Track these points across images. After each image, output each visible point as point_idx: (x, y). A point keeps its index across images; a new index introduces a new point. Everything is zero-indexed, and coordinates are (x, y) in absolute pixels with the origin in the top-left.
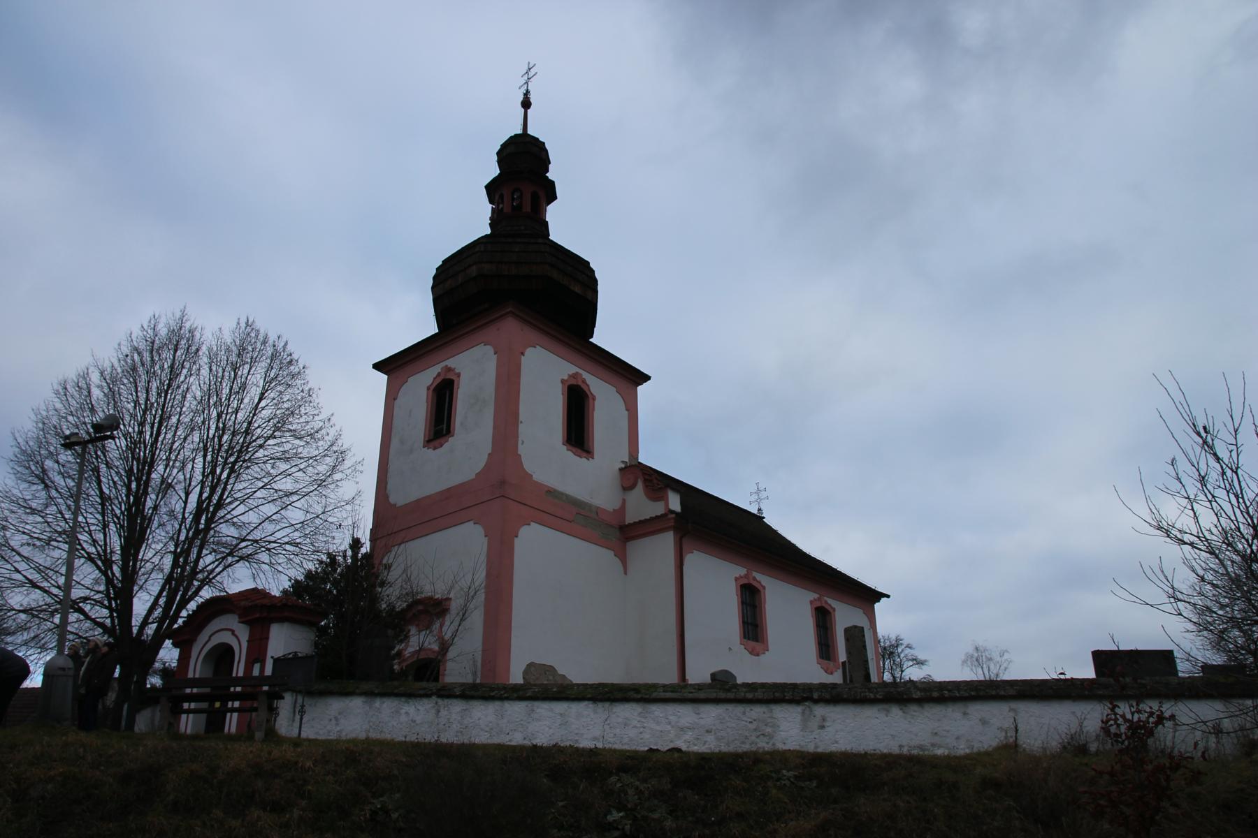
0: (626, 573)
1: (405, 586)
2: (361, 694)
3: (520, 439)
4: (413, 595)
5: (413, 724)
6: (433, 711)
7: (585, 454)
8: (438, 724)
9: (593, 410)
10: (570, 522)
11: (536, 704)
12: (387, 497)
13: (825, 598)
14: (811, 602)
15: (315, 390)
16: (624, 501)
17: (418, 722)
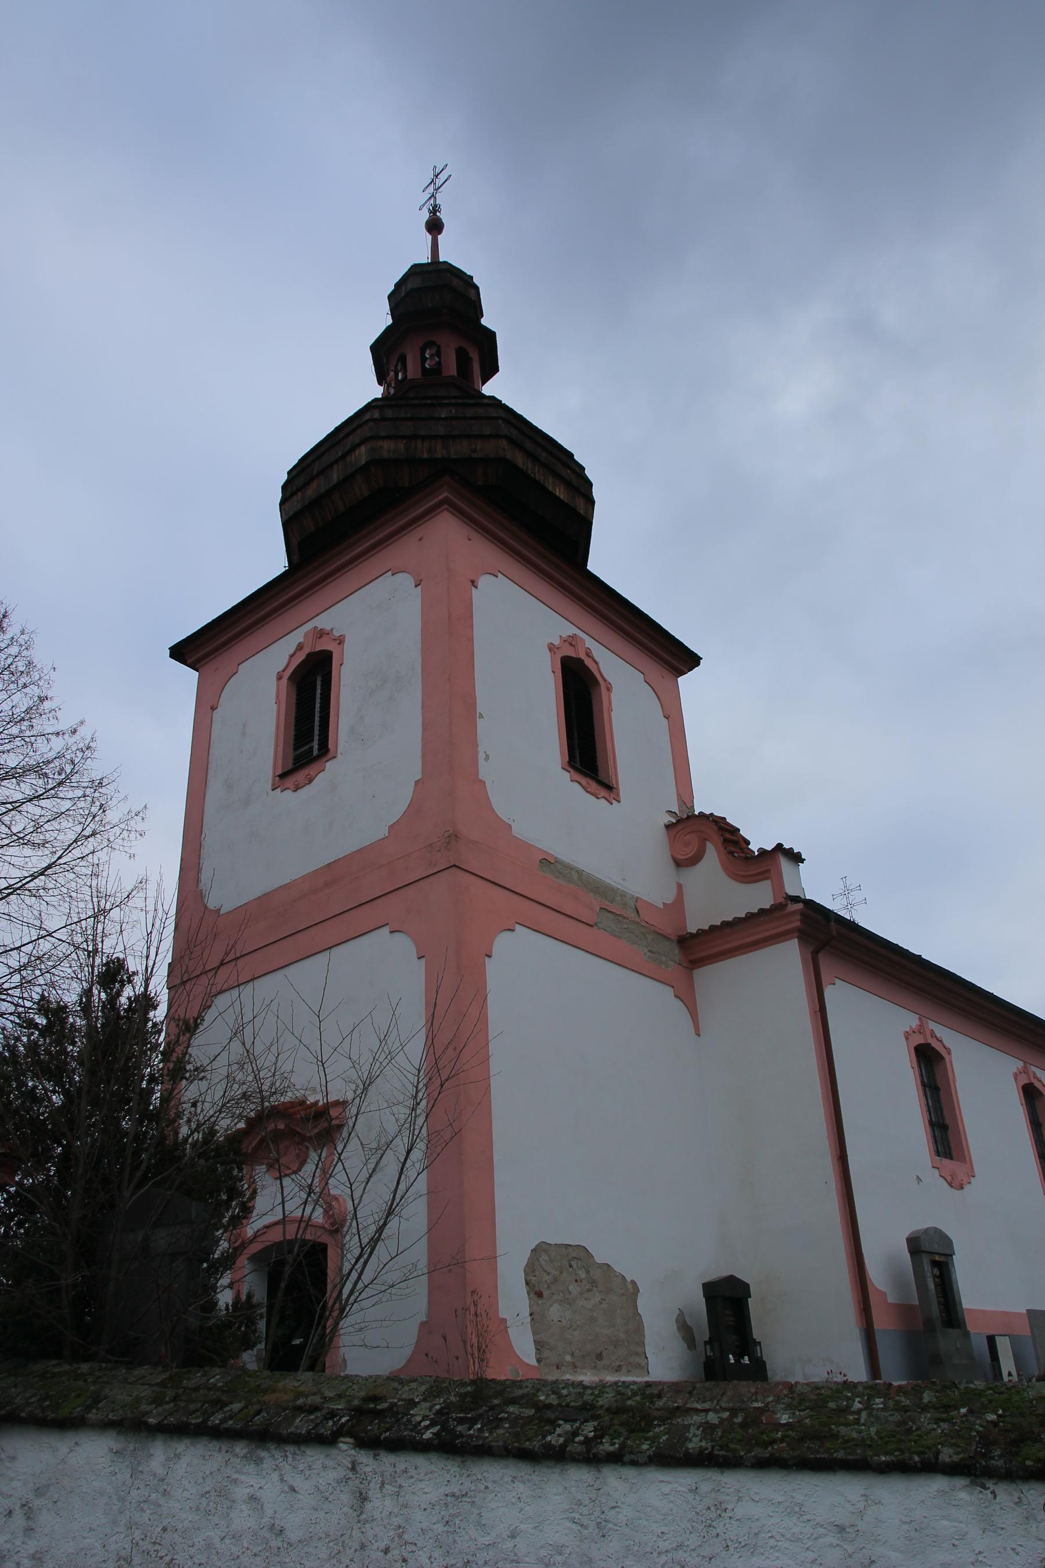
0: (699, 1035)
1: (240, 1076)
2: (106, 1426)
3: (481, 750)
4: (263, 1099)
5: (276, 1543)
6: (346, 1497)
7: (603, 792)
8: (363, 1547)
9: (610, 710)
10: (592, 926)
11: (732, 1481)
12: (200, 896)
13: (1033, 1068)
14: (1016, 1076)
15: (45, 672)
16: (680, 887)
17: (293, 1535)
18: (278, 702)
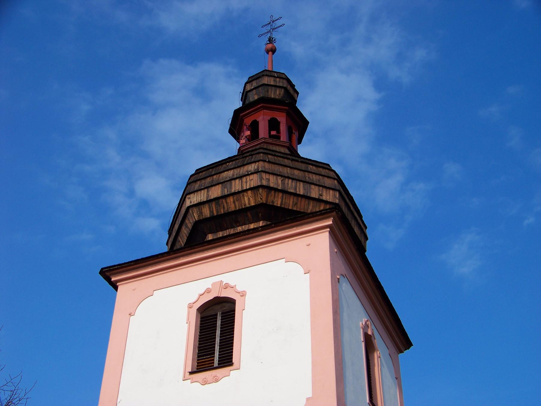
18: (188, 322)
